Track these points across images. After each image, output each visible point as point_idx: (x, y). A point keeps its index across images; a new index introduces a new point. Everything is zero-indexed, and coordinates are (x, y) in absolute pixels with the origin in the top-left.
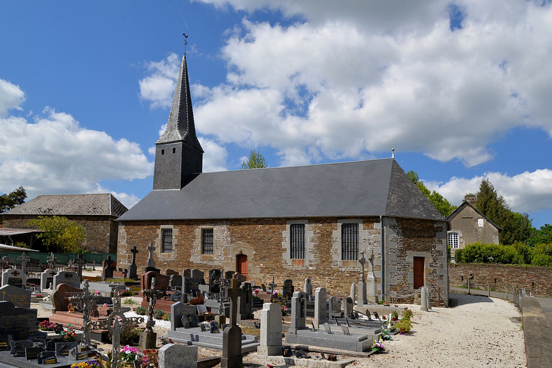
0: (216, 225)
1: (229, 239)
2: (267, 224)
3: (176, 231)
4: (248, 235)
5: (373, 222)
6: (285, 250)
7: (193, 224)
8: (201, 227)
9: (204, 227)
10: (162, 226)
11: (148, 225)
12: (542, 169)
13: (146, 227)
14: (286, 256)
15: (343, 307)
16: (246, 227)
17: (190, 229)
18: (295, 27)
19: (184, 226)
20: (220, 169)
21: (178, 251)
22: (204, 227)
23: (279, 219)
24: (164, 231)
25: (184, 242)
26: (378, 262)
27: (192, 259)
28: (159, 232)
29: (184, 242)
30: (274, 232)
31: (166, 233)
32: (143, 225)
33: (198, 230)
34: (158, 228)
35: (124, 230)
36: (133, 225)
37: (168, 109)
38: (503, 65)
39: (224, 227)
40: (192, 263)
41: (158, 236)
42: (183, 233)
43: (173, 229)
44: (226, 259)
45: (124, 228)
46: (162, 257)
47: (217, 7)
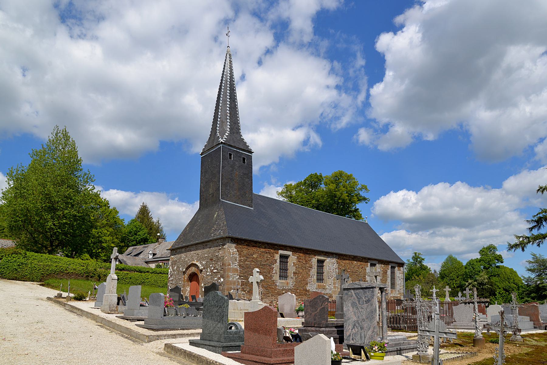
0: (328, 257)
2: (359, 261)
3: (293, 259)
4: (349, 269)
5: (278, 249)
7: (309, 254)
8: (317, 257)
9: (320, 258)
10: (281, 252)
11: (265, 248)
13: (262, 250)
14: (276, 277)
16: (347, 261)
17: (307, 258)
18: (485, 188)
19: (301, 254)
20: (281, 199)
21: (296, 278)
22: (320, 258)
23: (365, 258)
24: (282, 256)
26: (159, 270)
27: (308, 288)
28: (277, 257)
31: (284, 258)
32: (259, 247)
33: (314, 260)
35: (235, 250)
36: (247, 245)
37: (305, 142)
38: (24, 70)
39: (334, 260)
40: (308, 291)
41: (276, 262)
43: (291, 255)
45: (236, 248)
46: (281, 285)
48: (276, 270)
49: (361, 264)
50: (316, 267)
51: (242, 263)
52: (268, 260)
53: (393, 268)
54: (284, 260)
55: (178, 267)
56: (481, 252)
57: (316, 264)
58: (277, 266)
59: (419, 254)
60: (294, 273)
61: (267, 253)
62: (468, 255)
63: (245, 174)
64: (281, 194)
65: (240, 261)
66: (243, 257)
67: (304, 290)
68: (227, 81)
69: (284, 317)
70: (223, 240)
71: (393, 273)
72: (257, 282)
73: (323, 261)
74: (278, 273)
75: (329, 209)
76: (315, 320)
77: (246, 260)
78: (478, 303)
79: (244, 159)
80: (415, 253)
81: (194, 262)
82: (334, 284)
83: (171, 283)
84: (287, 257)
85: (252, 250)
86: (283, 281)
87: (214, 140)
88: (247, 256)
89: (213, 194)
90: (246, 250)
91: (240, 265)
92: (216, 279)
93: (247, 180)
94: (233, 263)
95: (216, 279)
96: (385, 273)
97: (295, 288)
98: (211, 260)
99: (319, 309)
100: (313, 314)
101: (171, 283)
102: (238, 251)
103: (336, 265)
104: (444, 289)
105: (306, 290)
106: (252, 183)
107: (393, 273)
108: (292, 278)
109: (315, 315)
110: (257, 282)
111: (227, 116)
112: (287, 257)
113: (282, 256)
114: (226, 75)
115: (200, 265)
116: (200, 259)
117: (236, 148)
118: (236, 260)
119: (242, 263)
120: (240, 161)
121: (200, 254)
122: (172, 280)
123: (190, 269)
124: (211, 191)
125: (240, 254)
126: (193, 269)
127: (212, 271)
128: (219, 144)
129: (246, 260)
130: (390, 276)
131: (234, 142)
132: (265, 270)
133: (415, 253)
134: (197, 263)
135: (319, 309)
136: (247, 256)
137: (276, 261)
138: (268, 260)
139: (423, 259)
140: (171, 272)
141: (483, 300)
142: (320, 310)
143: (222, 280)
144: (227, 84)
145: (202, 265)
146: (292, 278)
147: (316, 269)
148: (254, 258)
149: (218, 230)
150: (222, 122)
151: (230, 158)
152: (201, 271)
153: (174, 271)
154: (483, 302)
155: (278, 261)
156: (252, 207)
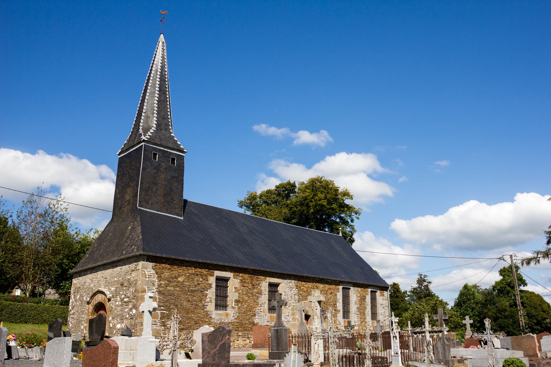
1: (296, 297)
3: (234, 282)
6: (339, 311)
10: (218, 273)
11: (196, 267)
12: (431, 215)
14: (211, 307)
15: (418, 330)
20: (242, 211)
21: (239, 308)
24: (218, 279)
25: (246, 298)
27: (256, 320)
28: (212, 280)
29: (246, 298)
30: (332, 293)
31: (222, 283)
33: (264, 284)
34: (211, 275)
35: (153, 272)
39: (293, 283)
42: (245, 285)
43: (232, 278)
44: (294, 319)
46: (217, 318)
47: (282, 162)
48: (211, 298)
49: (330, 289)
50: (267, 293)
51: (161, 289)
52: (199, 284)
53: (346, 291)
54: (222, 283)
55: (82, 296)
56: (502, 272)
57: (267, 290)
58: (211, 293)
59: (425, 276)
60: (237, 302)
61: (197, 275)
62: (486, 278)
63: (173, 177)
64: (241, 204)
65: (160, 286)
66: (164, 280)
67: (250, 323)
68: (157, 71)
69: (191, 359)
70: (137, 258)
71: (373, 299)
72: (149, 311)
73: (277, 285)
74: (214, 302)
75: (304, 221)
76: (214, 360)
77: (167, 285)
78: (430, 332)
79: (173, 160)
80: (421, 275)
81: (100, 289)
82: (293, 314)
83: (72, 318)
84: (226, 280)
85: (177, 270)
86: (221, 312)
87: (135, 138)
88: (170, 281)
89: (129, 200)
90: (168, 271)
91: (159, 292)
92: (126, 310)
93: (176, 184)
94: (149, 290)
95: (126, 310)
96: (363, 299)
97: (238, 321)
98: (122, 285)
99: (218, 346)
100: (212, 352)
101: (72, 318)
102: (157, 273)
103: (295, 291)
104: (464, 322)
105: (254, 324)
106: (183, 188)
107: (373, 299)
108: (233, 308)
109: (215, 354)
110: (149, 311)
111: (154, 110)
112: (226, 280)
113: (218, 279)
114: (156, 65)
115: (107, 293)
116: (108, 284)
117: (164, 147)
118: (154, 285)
119: (161, 289)
120: (168, 161)
121: (109, 277)
122: (74, 314)
123: (96, 297)
124: (127, 197)
125: (160, 277)
126: (99, 298)
127: (122, 300)
128: (141, 142)
129: (167, 285)
130: (369, 304)
131: (161, 140)
132: (195, 298)
133: (421, 275)
134: (104, 290)
135: (218, 346)
136: (170, 281)
137: (210, 285)
138: (199, 284)
139: (430, 283)
140: (73, 302)
141: (435, 329)
142: (220, 347)
143: (134, 311)
144: (157, 74)
145: (111, 292)
146: (233, 308)
147: (267, 296)
148: (179, 282)
149: (132, 246)
150: (147, 117)
151: (155, 158)
152: (109, 300)
153: (76, 301)
154: (436, 332)
155: (214, 286)
156: (181, 216)
